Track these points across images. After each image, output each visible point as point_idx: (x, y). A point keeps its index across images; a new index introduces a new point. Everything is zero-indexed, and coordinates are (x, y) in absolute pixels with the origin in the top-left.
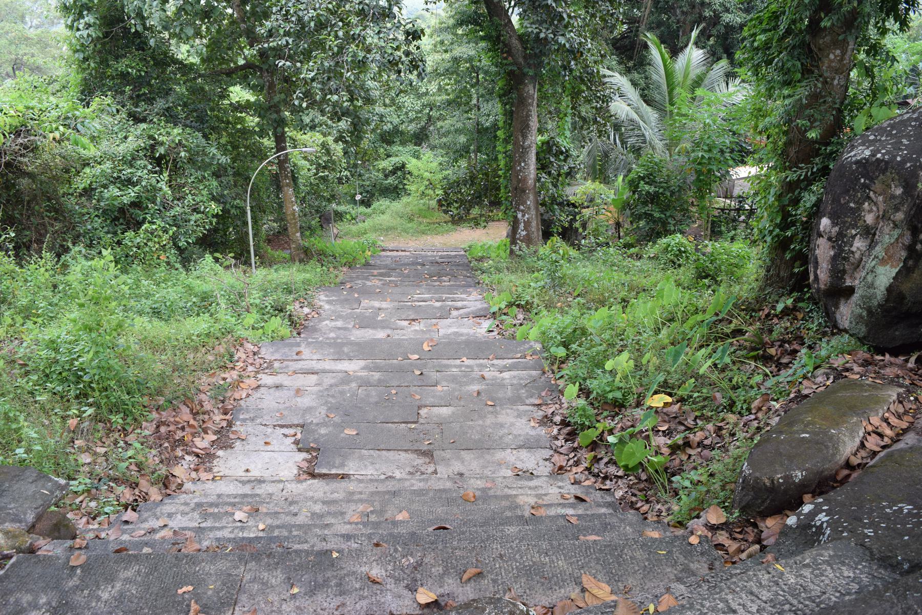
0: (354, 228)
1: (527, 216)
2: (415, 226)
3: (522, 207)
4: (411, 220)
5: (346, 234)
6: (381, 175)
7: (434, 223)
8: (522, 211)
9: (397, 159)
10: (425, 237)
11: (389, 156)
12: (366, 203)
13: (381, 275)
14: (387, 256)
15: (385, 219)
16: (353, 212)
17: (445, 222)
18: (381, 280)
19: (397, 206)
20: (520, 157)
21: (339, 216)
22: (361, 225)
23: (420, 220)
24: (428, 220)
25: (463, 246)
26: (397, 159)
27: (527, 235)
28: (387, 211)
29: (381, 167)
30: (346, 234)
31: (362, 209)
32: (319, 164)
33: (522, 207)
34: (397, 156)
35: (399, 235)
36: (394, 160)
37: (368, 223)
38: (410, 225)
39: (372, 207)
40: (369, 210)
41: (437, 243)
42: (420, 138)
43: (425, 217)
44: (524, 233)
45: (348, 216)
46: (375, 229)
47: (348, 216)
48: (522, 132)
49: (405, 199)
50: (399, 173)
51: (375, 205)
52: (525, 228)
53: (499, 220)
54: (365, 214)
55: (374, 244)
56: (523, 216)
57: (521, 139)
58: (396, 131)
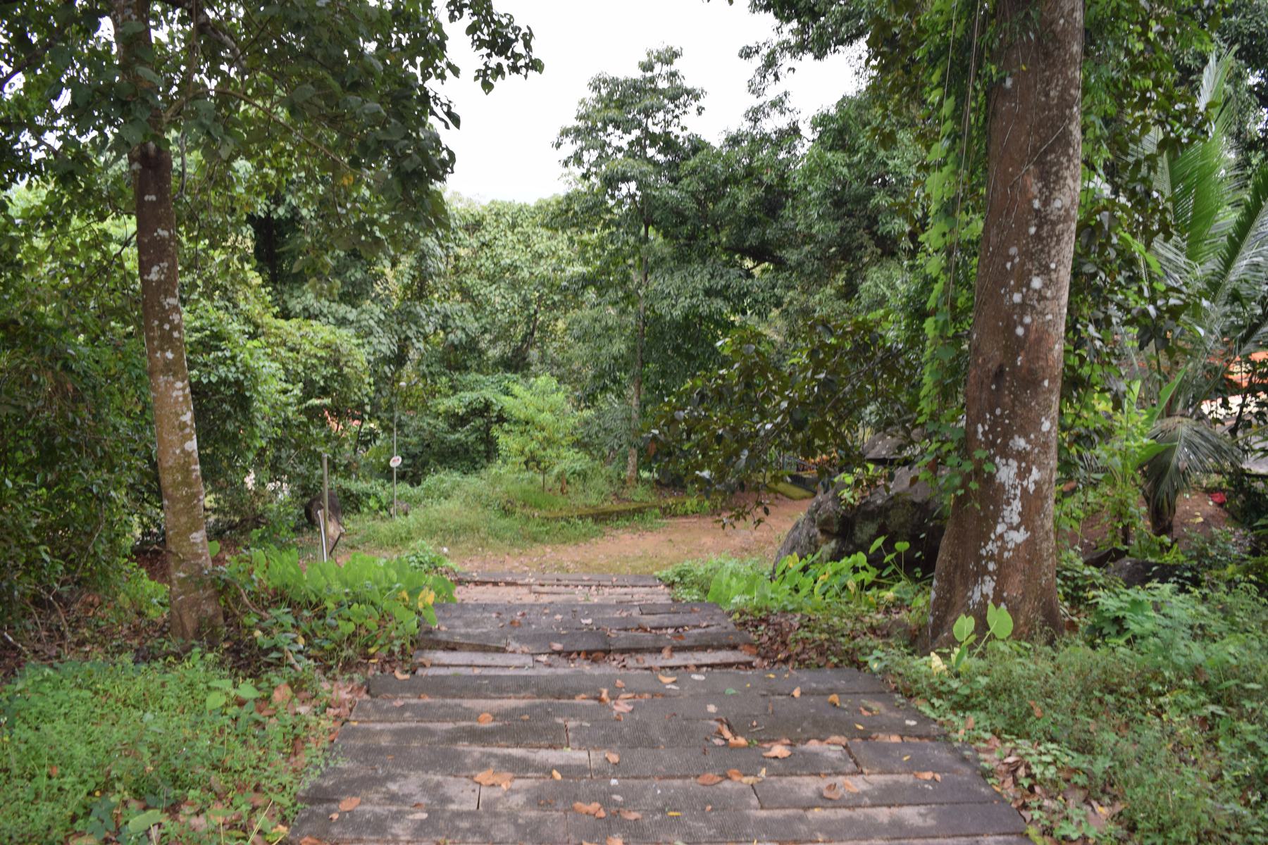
0: (384, 528)
1: (1035, 474)
2: (517, 525)
3: (1020, 443)
4: (506, 512)
5: (366, 540)
6: (442, 424)
7: (557, 519)
8: (1021, 456)
9: (474, 395)
10: (538, 548)
11: (455, 389)
12: (411, 475)
13: (514, 729)
14: (485, 607)
15: (450, 509)
16: (383, 495)
17: (580, 517)
18: (520, 767)
19: (473, 483)
20: (1027, 255)
21: (349, 503)
22: (400, 520)
23: (527, 511)
24: (544, 513)
25: (662, 574)
26: (474, 395)
27: (1030, 543)
28: (453, 495)
29: (442, 408)
30: (366, 540)
31: (403, 488)
32: (313, 382)
33: (1020, 443)
34: (472, 389)
35: (484, 543)
36: (468, 396)
37: (414, 518)
38: (505, 522)
39: (424, 484)
40: (416, 491)
41: (567, 562)
42: (516, 363)
43: (538, 506)
44: (1019, 537)
45: (372, 503)
46: (430, 531)
47: (372, 503)
48: (1041, 163)
49: (496, 468)
50: (479, 422)
51: (429, 481)
52: (1027, 519)
53: (686, 515)
54: (408, 500)
55: (434, 566)
56: (1023, 474)
57: (1035, 187)
58: (471, 346)
